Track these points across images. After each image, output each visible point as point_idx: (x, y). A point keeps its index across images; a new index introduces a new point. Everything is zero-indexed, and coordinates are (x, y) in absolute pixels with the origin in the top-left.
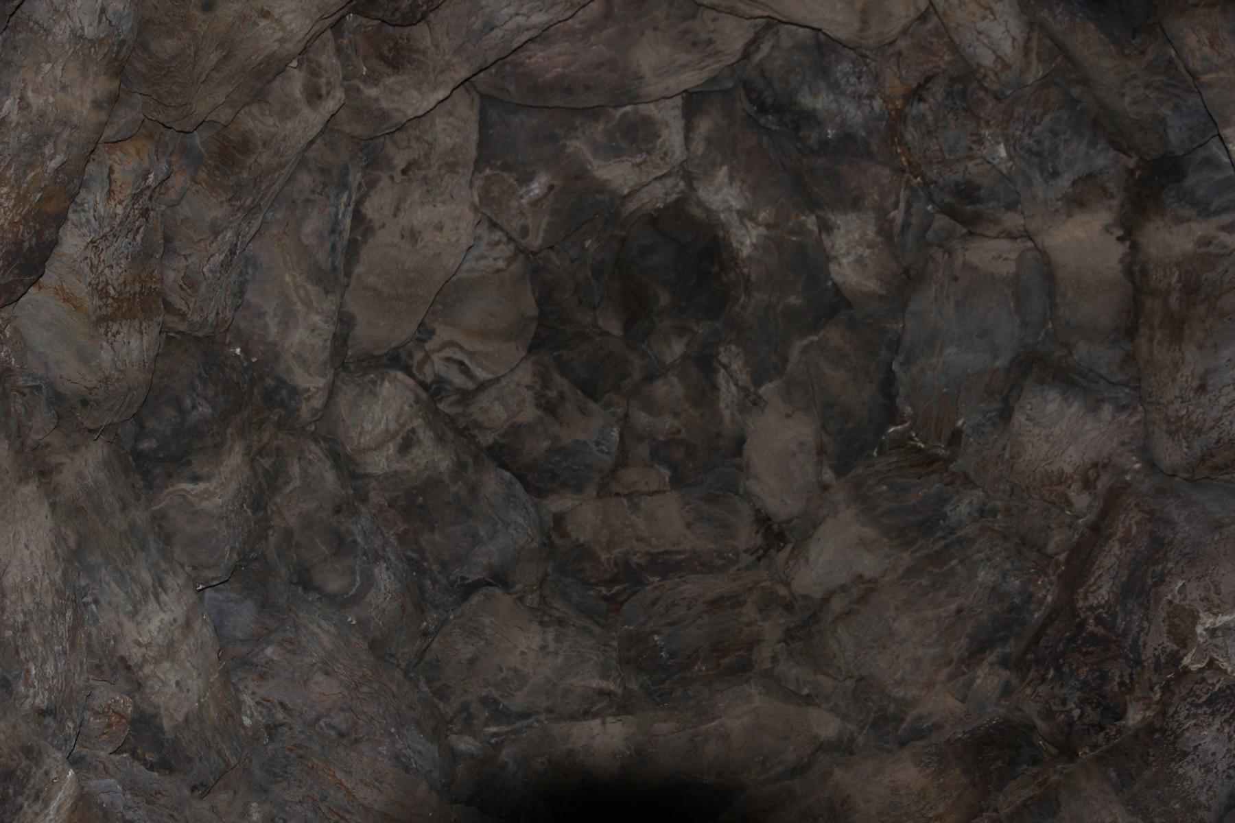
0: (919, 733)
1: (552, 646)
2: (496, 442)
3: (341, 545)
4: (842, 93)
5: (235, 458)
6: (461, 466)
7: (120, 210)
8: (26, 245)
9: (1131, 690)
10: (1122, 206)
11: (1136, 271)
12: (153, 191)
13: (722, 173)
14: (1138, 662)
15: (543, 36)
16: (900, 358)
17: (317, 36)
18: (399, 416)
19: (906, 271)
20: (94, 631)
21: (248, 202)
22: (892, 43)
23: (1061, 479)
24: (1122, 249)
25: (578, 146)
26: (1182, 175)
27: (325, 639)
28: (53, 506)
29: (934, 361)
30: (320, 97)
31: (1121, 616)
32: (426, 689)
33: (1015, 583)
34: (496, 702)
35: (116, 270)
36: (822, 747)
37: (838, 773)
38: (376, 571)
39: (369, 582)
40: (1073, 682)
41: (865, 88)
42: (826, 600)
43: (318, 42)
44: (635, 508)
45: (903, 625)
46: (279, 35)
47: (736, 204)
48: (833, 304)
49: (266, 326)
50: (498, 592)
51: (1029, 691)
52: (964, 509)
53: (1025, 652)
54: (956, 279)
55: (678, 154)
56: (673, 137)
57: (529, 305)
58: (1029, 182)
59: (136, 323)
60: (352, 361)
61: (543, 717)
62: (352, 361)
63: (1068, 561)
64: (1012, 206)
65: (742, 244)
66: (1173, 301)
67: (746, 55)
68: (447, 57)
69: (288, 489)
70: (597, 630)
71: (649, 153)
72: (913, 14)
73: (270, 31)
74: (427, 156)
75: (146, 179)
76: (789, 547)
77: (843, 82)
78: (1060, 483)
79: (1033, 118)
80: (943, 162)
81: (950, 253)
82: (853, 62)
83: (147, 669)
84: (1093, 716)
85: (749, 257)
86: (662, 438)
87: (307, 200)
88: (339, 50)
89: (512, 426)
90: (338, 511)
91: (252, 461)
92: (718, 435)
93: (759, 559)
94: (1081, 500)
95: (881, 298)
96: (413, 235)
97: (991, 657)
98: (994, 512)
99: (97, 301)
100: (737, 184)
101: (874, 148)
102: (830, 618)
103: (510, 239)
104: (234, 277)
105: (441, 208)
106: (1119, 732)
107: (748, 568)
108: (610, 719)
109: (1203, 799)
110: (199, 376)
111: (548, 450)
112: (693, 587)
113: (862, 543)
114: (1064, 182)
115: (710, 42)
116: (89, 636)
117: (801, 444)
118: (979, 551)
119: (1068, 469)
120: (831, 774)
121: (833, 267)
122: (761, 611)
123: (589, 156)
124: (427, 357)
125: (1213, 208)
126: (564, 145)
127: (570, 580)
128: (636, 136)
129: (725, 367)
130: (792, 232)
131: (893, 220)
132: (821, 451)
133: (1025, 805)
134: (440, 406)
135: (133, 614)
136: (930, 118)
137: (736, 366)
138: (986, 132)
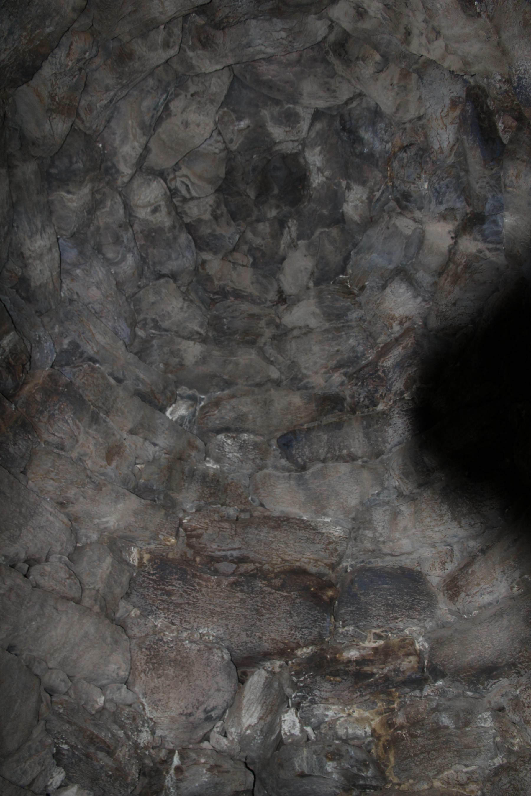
0: (306, 388)
1: (185, 309)
2: (190, 222)
3: (117, 240)
4: (377, 136)
5: (86, 190)
6: (174, 227)
7: (70, 64)
8: (27, 64)
9: (383, 399)
10: (458, 225)
11: (452, 251)
12: (86, 61)
13: (318, 149)
14: (390, 390)
15: (269, 59)
16: (356, 250)
17: (175, 18)
18: (156, 197)
19: (371, 218)
20: (14, 238)
21: (124, 82)
22: (404, 123)
23: (393, 318)
24: (451, 242)
25: (265, 113)
26: (483, 223)
27: (100, 274)
28: (10, 182)
29: (367, 256)
30: (168, 47)
31: (391, 373)
32: (132, 307)
33: (361, 348)
34: (157, 322)
35: (62, 90)
36: (270, 380)
37: (272, 391)
38: (128, 256)
39: (124, 259)
40: (366, 389)
41: (386, 138)
42: (292, 329)
43: (175, 21)
44: (235, 269)
45: (316, 348)
46: (161, 10)
47: (318, 164)
48: (339, 220)
49: (115, 139)
50: (171, 281)
51: (349, 387)
52: (355, 315)
53: (354, 373)
54: (388, 228)
55: (304, 134)
56: (304, 125)
57: (222, 172)
58: (430, 202)
59: (63, 117)
60: (142, 167)
61: (173, 333)
62: (142, 167)
63: (382, 348)
64: (420, 209)
65: (314, 181)
66: (460, 269)
67: (347, 103)
68: (227, 51)
69: (103, 210)
70: (204, 309)
71: (293, 128)
72: (417, 115)
73: (157, 6)
74: (203, 92)
75: (85, 54)
76: (286, 305)
77: (379, 131)
78: (392, 319)
79: (443, 177)
80: (403, 181)
81: (390, 217)
82: (386, 125)
83: (30, 261)
84: (367, 402)
85: (315, 188)
86: (254, 246)
87: (148, 91)
88: (183, 28)
89: (199, 219)
90: (120, 226)
91: (93, 194)
92: (276, 253)
93: (273, 305)
94: (396, 328)
95: (358, 224)
96: (186, 124)
97: (342, 371)
98: (364, 321)
99: (49, 101)
100: (322, 156)
101: (380, 163)
102: (291, 336)
103: (224, 142)
104: (108, 113)
105: (202, 117)
106: (373, 410)
107: (268, 307)
108: (197, 343)
109: (389, 440)
110: (82, 150)
111: (209, 234)
112: (245, 307)
113: (313, 314)
114: (442, 208)
115: (334, 91)
116: (11, 239)
117: (306, 269)
118: (353, 332)
119: (397, 315)
120: (270, 390)
121: (345, 205)
122: (267, 324)
123: (269, 119)
124: (175, 178)
125: (488, 240)
126: (260, 111)
127: (200, 287)
128: (290, 119)
129: (289, 228)
130: (335, 184)
131: (375, 196)
132: (312, 274)
133: (331, 423)
134: (174, 200)
135: (30, 237)
136: (405, 161)
137: (293, 229)
138: (423, 176)
